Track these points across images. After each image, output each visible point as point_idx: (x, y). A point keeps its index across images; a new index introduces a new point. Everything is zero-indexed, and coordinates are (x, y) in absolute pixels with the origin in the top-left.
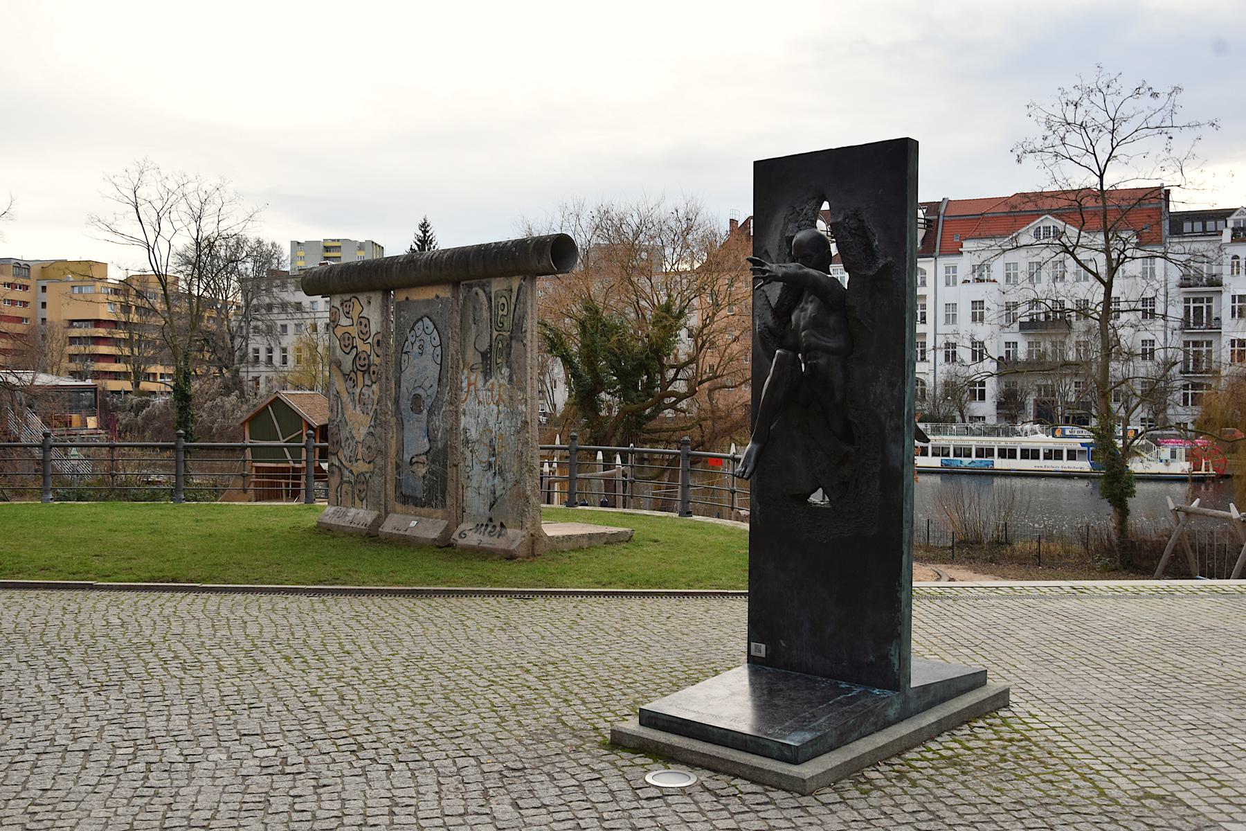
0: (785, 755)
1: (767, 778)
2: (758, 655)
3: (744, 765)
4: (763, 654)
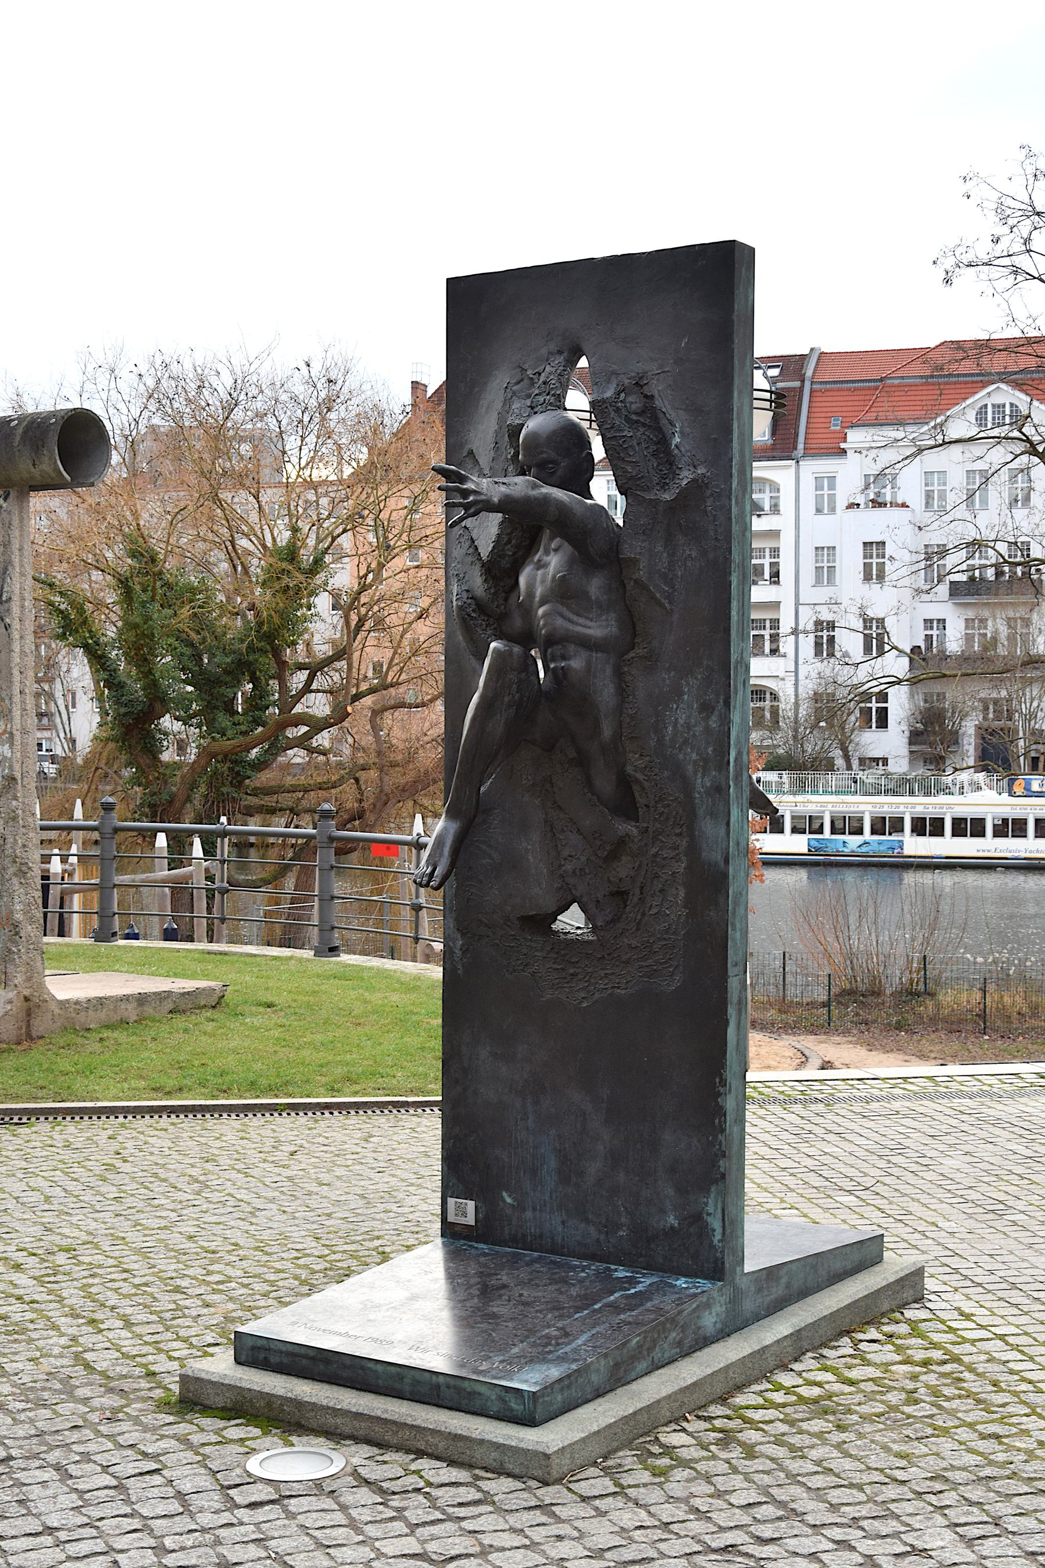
0: (512, 1410)
1: (479, 1454)
2: (462, 1220)
3: (435, 1432)
4: (470, 1220)
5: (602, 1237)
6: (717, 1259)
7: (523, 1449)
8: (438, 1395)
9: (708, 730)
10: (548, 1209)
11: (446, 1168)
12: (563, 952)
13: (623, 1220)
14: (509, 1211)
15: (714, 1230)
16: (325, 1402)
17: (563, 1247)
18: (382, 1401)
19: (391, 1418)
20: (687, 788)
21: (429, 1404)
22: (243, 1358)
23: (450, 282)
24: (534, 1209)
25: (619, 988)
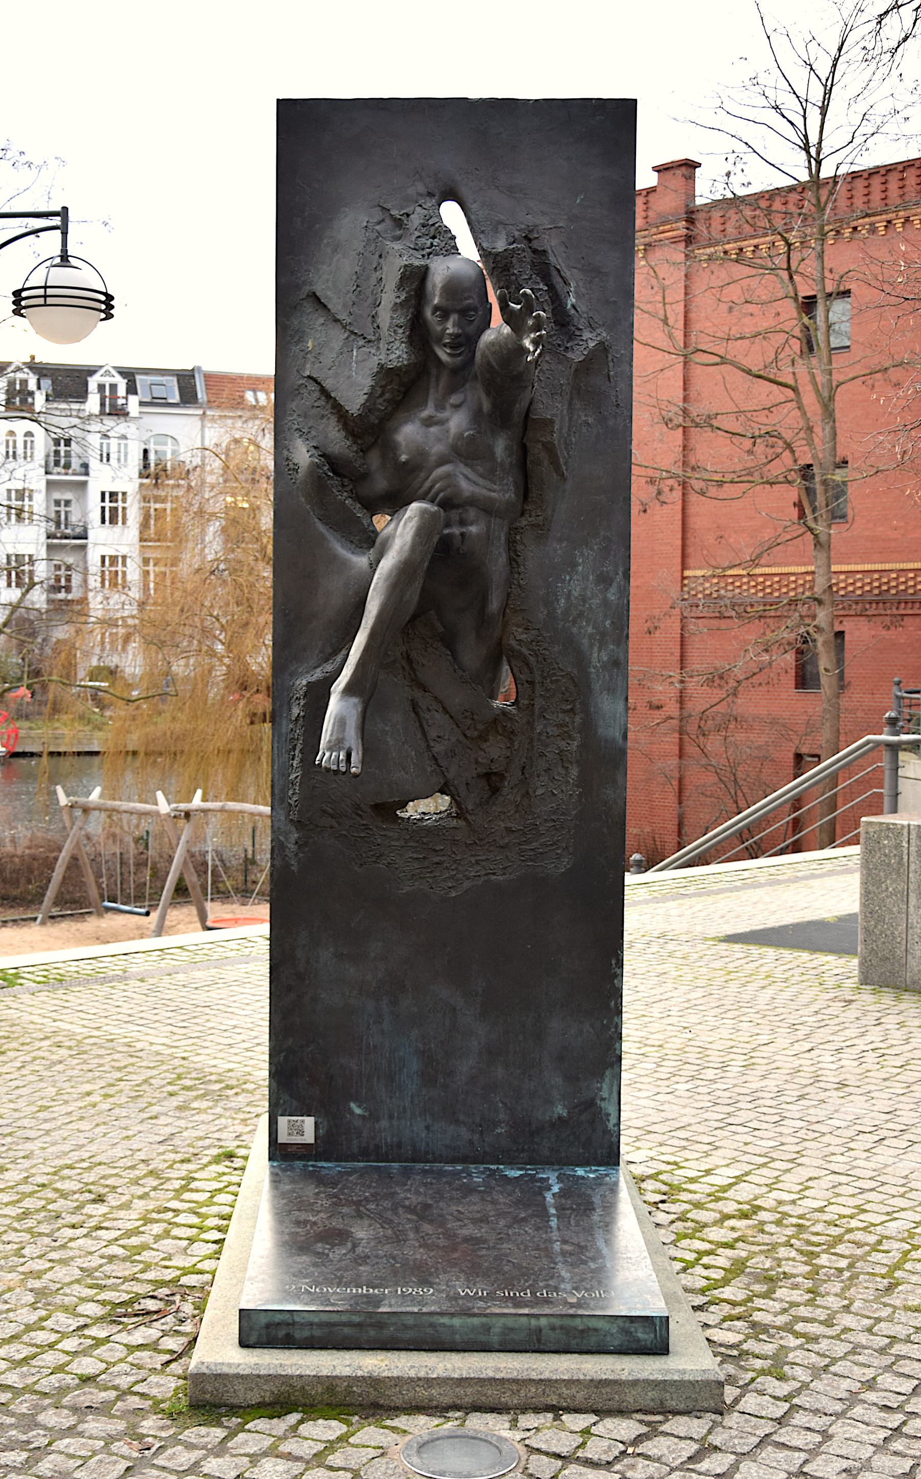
0: (639, 1340)
1: (630, 1398)
2: (298, 1140)
3: (569, 1383)
4: (309, 1137)
5: (476, 1137)
6: (612, 1143)
7: (690, 1382)
8: (539, 1341)
9: (606, 603)
10: (408, 1114)
11: (275, 1085)
12: (425, 840)
13: (501, 1116)
14: (358, 1123)
15: (609, 1115)
16: (412, 1374)
17: (427, 1153)
18: (329, 1358)
19: (510, 1376)
20: (582, 662)
21: (527, 1351)
22: (253, 1339)
23: (278, 100)
24: (391, 1117)
25: (494, 874)
